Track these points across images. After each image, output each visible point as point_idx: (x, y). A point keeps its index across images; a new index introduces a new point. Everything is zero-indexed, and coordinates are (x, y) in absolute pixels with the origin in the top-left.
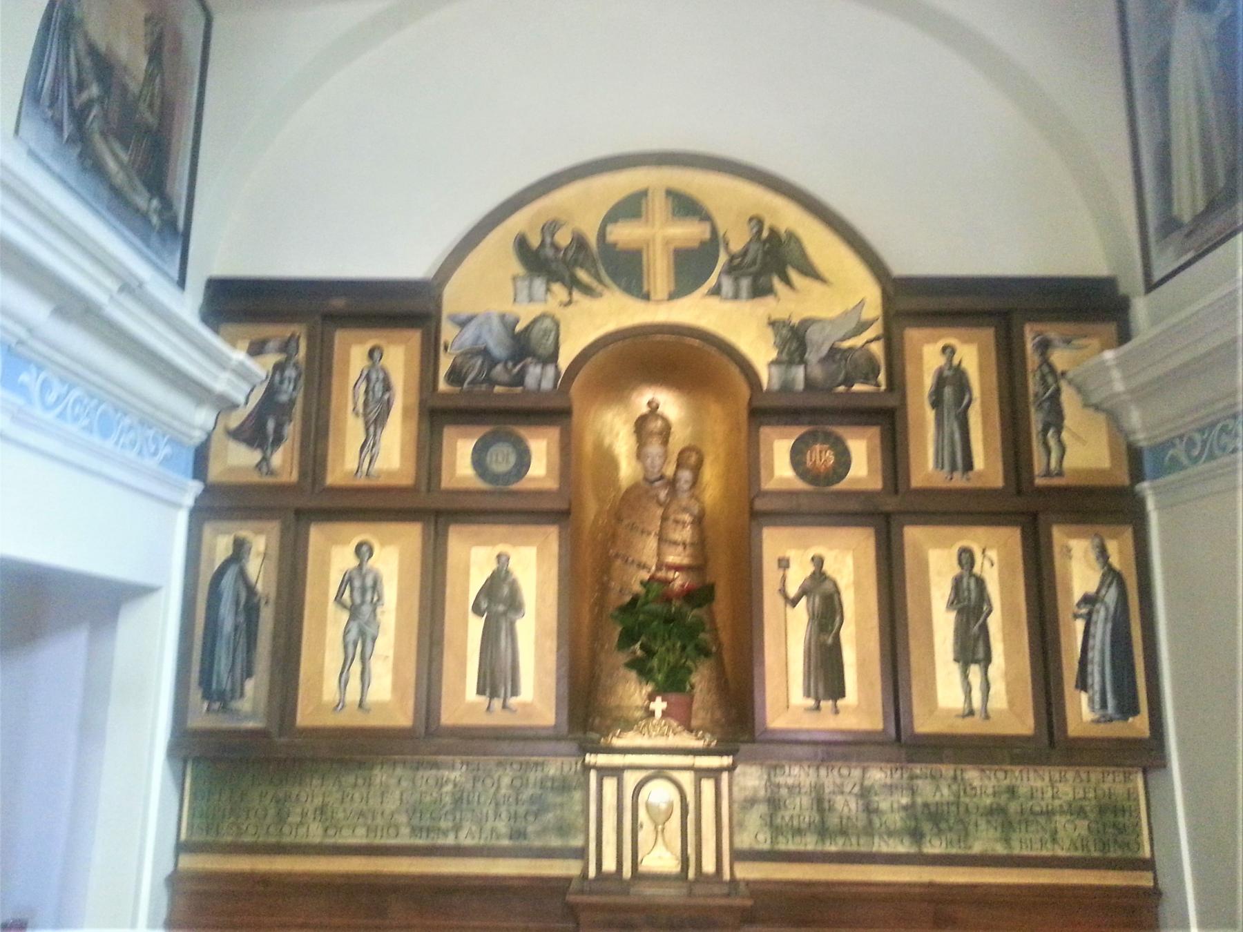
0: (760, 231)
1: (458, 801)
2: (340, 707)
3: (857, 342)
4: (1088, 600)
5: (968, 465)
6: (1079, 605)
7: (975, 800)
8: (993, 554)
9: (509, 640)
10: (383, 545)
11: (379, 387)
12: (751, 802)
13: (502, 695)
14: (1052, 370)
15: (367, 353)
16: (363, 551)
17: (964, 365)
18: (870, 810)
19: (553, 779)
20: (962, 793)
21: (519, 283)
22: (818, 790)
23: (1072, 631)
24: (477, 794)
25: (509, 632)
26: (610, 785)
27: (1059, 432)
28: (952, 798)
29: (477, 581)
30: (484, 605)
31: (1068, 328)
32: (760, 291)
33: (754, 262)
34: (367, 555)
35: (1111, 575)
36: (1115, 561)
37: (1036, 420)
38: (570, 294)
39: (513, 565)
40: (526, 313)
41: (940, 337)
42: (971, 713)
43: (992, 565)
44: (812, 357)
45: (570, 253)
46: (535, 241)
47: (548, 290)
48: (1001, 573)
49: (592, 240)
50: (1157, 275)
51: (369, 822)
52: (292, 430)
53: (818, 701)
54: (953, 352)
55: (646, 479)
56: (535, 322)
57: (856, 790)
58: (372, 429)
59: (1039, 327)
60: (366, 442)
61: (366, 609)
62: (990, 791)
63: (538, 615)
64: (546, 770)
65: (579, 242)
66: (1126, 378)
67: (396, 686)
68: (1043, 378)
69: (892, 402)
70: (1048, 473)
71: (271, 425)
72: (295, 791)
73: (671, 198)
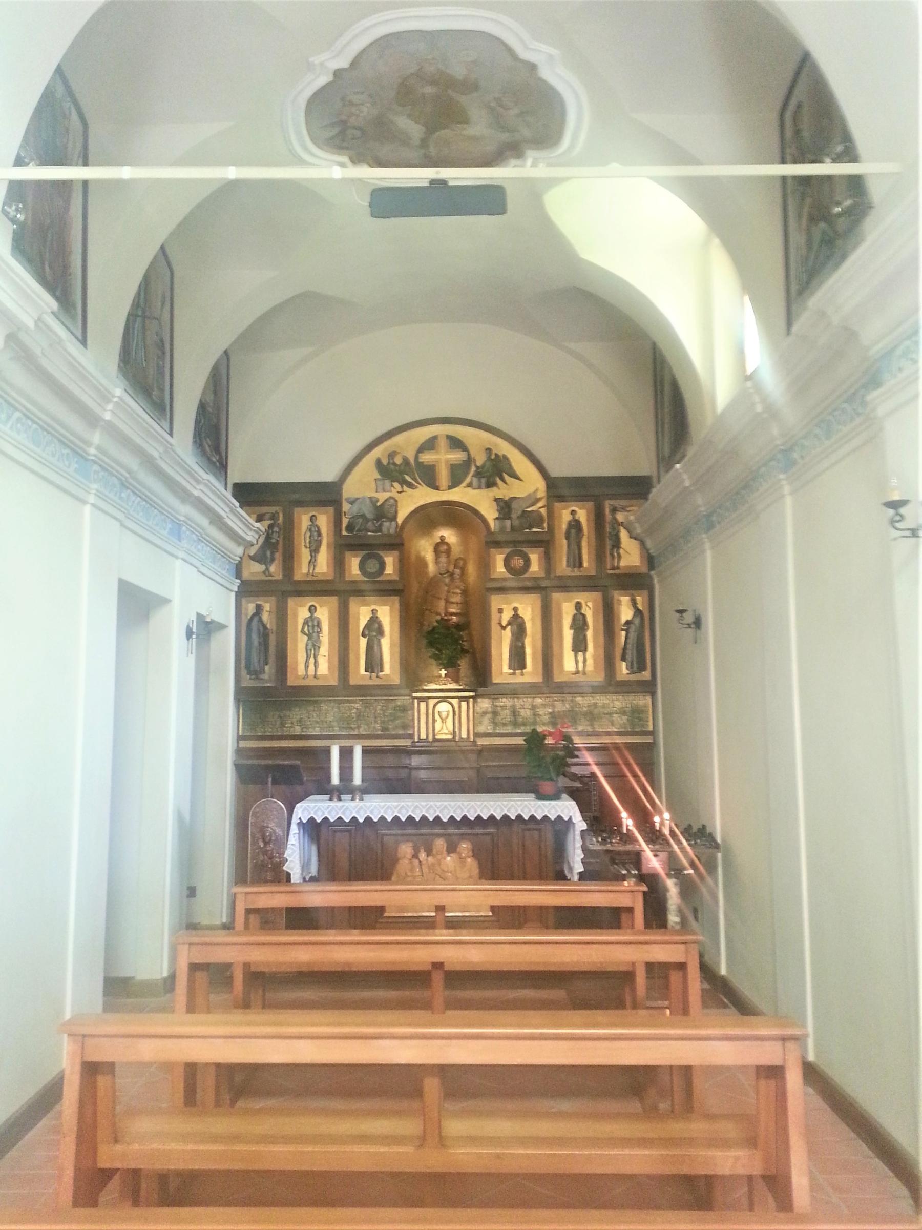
4: (628, 623)
5: (581, 565)
12: (485, 713)
16: (312, 609)
19: (399, 706)
22: (513, 707)
26: (423, 705)
29: (363, 622)
30: (367, 633)
32: (490, 485)
38: (402, 487)
40: (382, 497)
44: (514, 516)
46: (385, 462)
49: (412, 461)
56: (386, 501)
65: (406, 461)
72: (288, 713)
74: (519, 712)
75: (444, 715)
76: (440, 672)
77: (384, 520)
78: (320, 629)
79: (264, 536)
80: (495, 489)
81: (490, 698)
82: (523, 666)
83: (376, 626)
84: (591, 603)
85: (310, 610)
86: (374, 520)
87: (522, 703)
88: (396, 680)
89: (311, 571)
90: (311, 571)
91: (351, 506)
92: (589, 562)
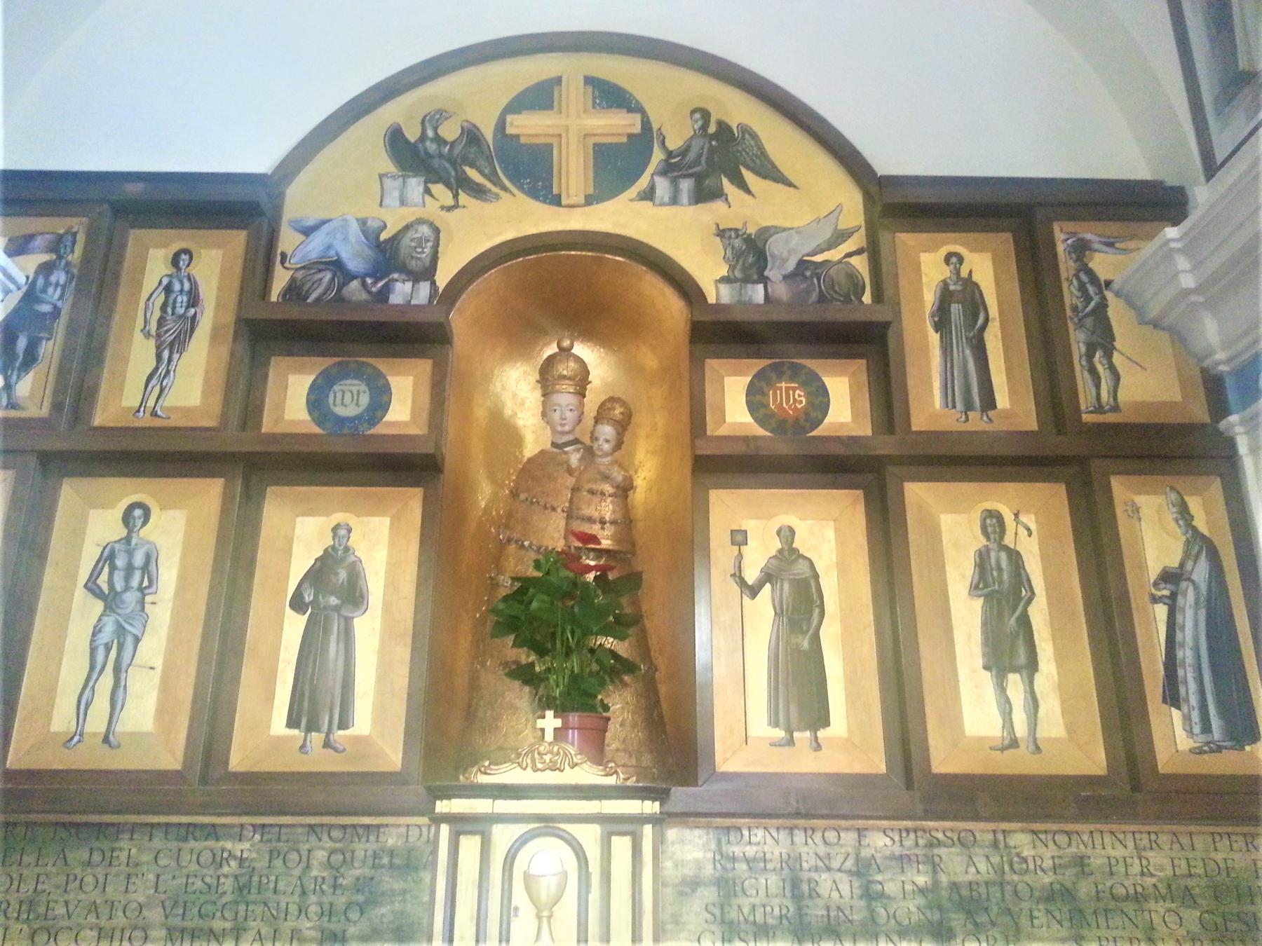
0: (704, 127)
1: (241, 889)
2: (76, 739)
3: (834, 255)
4: (1170, 577)
5: (989, 402)
6: (1156, 584)
7: (1026, 878)
8: (1029, 519)
9: (342, 645)
10: (163, 508)
11: (182, 299)
12: (693, 884)
13: (325, 728)
14: (1094, 279)
15: (171, 256)
16: (135, 516)
17: (975, 278)
18: (870, 895)
19: (392, 853)
20: (1007, 868)
21: (388, 183)
22: (792, 864)
23: (1151, 621)
24: (273, 878)
25: (342, 637)
26: (470, 846)
27: (1108, 355)
28: (992, 876)
29: (301, 564)
30: (308, 597)
31: (1113, 228)
32: (705, 194)
33: (696, 162)
34: (139, 522)
35: (1199, 543)
36: (1200, 523)
37: (1078, 340)
38: (456, 196)
39: (354, 541)
40: (393, 219)
41: (944, 244)
42: (1014, 743)
43: (1030, 535)
44: (773, 273)
45: (458, 149)
46: (412, 134)
47: (428, 191)
48: (1041, 543)
49: (488, 133)
50: (1220, 156)
51: (103, 922)
52: (50, 349)
53: (790, 732)
54: (961, 260)
55: (554, 445)
56: (407, 228)
57: (849, 864)
58: (166, 354)
59: (1070, 226)
60: (156, 369)
61: (131, 598)
62: (1048, 863)
63: (387, 608)
64: (382, 838)
65: (472, 136)
66: (1195, 267)
67: (161, 711)
68: (1082, 288)
69: (880, 315)
70: (1099, 409)
71: (22, 343)
73: (590, 89)
74: (809, 881)
75: (546, 889)
76: (540, 723)
77: (396, 276)
78: (150, 581)
79: (20, 294)
80: (718, 206)
81: (707, 827)
82: (821, 718)
83: (343, 575)
84: (1033, 517)
85: (127, 518)
86: (367, 275)
87: (822, 850)
88: (392, 756)
89: (151, 403)
90: (151, 403)
91: (302, 238)
92: (1012, 391)
